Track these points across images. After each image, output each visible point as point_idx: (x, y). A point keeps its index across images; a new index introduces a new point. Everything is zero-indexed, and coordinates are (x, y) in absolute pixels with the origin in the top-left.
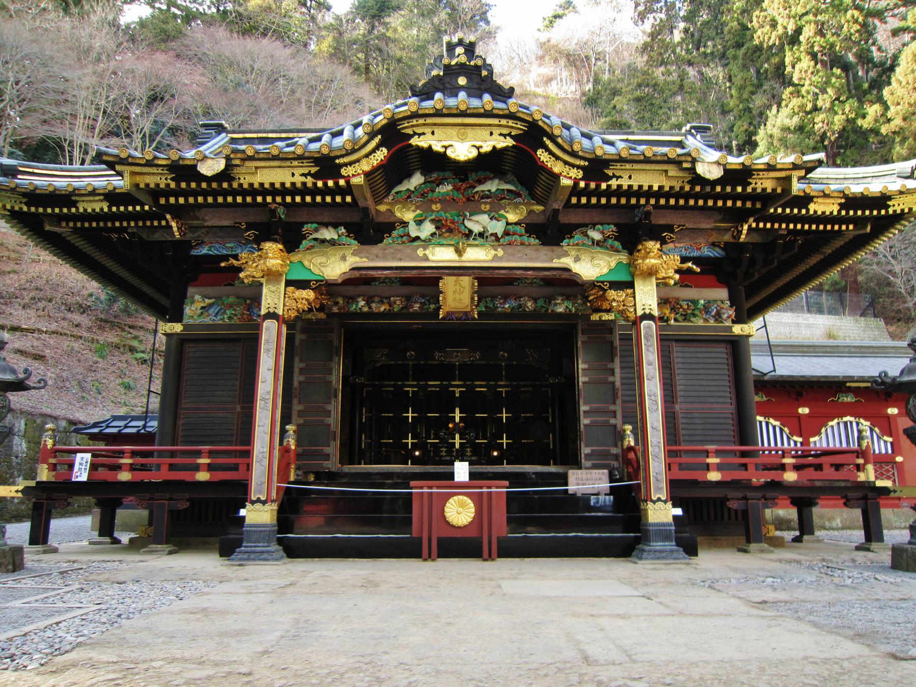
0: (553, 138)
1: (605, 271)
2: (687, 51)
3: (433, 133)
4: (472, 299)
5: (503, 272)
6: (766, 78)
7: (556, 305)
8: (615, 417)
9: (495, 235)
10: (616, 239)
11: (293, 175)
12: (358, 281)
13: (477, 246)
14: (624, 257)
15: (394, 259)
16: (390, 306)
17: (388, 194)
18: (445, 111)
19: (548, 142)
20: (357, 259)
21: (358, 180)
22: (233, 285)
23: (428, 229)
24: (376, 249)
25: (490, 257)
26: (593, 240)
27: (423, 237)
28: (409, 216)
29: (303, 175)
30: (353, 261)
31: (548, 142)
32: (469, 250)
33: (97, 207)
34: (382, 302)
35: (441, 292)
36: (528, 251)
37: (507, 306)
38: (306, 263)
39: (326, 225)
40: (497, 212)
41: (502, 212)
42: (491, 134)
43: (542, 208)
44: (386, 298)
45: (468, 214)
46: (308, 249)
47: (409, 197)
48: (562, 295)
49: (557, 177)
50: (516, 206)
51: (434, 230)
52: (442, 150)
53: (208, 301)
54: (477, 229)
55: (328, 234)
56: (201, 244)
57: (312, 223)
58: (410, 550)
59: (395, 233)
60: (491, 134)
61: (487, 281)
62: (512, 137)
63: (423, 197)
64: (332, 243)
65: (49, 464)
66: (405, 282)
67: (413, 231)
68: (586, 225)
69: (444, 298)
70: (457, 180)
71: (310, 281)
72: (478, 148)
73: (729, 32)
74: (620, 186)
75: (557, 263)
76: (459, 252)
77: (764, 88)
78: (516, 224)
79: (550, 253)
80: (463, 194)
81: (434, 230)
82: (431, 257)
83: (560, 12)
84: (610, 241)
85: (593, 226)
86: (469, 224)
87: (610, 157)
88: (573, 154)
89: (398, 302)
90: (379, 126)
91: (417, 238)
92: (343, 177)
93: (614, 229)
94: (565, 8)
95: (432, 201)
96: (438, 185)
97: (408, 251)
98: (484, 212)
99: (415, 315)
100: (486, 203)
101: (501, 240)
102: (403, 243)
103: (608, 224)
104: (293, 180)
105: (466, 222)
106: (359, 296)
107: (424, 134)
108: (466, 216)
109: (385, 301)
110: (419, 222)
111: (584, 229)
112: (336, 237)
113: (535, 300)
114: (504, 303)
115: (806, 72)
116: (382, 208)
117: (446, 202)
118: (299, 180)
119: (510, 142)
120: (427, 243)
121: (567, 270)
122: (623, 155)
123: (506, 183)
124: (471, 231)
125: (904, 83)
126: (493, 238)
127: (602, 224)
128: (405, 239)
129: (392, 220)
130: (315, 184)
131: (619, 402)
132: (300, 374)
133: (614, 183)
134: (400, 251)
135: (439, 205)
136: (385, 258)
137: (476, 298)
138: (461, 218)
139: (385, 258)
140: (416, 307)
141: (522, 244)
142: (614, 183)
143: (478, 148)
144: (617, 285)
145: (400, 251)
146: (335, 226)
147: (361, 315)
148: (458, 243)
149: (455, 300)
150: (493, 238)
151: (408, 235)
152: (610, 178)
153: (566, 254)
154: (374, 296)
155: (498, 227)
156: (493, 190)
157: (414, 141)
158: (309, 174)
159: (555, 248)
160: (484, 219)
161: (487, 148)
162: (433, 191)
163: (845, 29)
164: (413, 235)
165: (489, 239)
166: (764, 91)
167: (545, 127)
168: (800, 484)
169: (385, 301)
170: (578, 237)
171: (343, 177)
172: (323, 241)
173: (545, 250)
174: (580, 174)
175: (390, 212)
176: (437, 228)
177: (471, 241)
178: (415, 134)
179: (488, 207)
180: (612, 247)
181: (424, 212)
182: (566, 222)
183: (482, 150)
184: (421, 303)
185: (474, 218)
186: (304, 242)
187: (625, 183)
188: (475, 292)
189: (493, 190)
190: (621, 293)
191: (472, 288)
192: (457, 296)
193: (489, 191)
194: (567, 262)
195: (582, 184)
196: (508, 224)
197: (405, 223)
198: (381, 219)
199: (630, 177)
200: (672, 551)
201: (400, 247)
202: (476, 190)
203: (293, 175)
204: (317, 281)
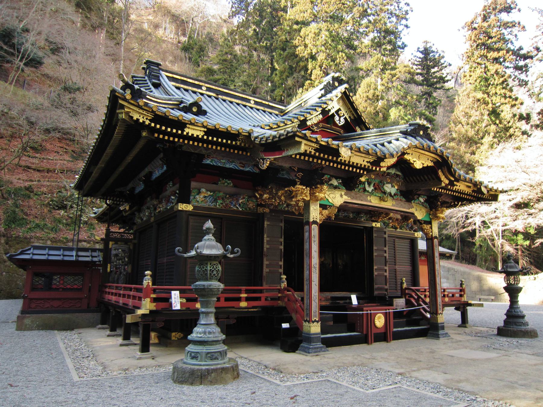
6: (295, 70)
8: (386, 272)
22: (217, 184)
33: (196, 133)
53: (209, 193)
56: (209, 156)
58: (364, 340)
65: (151, 298)
72: (423, 164)
73: (280, 41)
77: (294, 76)
115: (319, 76)
125: (362, 96)
131: (387, 265)
132: (267, 244)
143: (423, 164)
163: (338, 61)
166: (294, 78)
200: (321, 347)
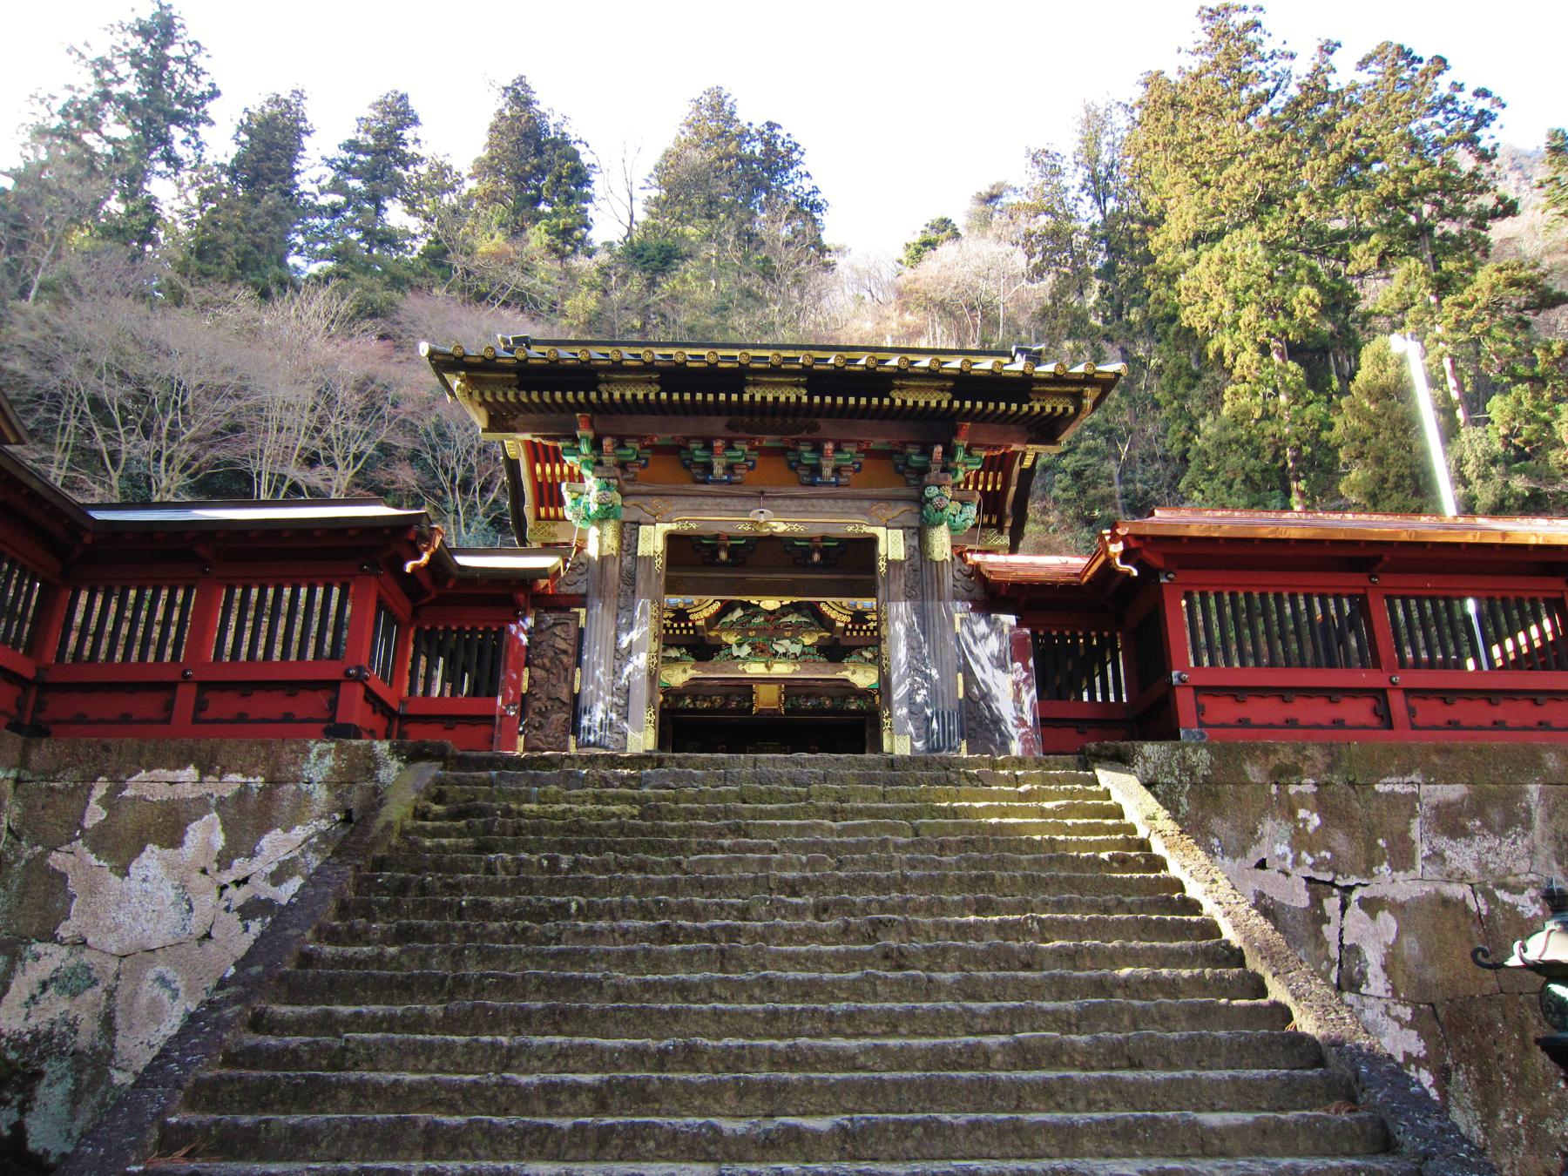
2: (1105, 321)
12: (693, 687)
23: (746, 649)
24: (708, 665)
28: (731, 639)
30: (692, 673)
49: (834, 621)
50: (810, 632)
54: (781, 650)
61: (790, 687)
63: (742, 627)
64: (676, 660)
75: (839, 675)
83: (933, 236)
85: (866, 648)
94: (939, 231)
99: (732, 711)
110: (740, 645)
113: (833, 699)
116: (713, 634)
120: (745, 660)
139: (715, 672)
140: (734, 705)
146: (678, 647)
147: (687, 711)
155: (797, 649)
160: (787, 642)
168: (506, 637)
173: (831, 666)
175: (719, 637)
192: (767, 698)
194: (846, 674)
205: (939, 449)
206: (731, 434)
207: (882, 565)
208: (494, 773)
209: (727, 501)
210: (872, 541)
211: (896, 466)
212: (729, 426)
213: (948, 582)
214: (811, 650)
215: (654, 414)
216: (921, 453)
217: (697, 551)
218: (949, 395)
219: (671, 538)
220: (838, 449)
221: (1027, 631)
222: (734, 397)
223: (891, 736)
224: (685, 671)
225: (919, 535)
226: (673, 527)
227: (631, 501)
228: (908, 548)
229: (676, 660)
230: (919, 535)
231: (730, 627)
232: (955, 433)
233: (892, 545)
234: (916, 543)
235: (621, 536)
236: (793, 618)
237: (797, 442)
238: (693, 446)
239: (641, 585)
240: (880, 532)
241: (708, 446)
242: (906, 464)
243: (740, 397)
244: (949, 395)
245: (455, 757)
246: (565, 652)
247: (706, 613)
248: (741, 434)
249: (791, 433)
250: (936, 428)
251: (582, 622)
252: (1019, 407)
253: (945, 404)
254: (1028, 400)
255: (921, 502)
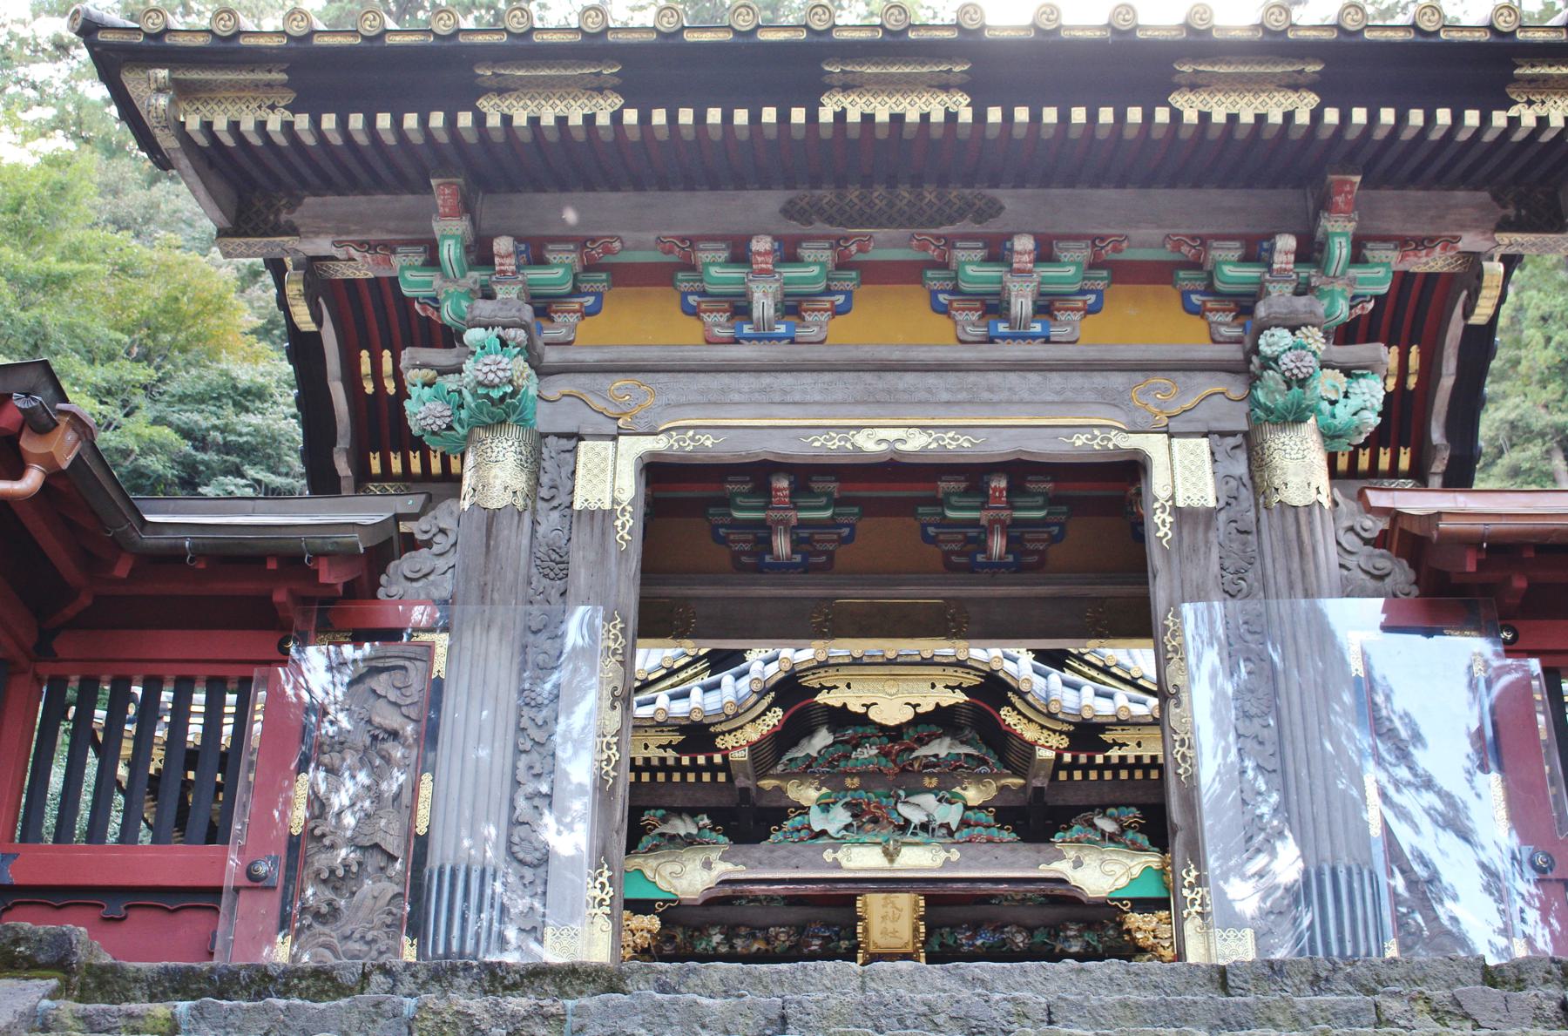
0: (1021, 695)
1: (1123, 882)
3: (849, 686)
4: (916, 929)
5: (960, 885)
7: (1067, 939)
9: (947, 826)
10: (1142, 830)
11: (646, 747)
13: (917, 844)
14: (1153, 860)
15: (787, 866)
16: (768, 943)
17: (776, 764)
18: (866, 660)
19: (1014, 699)
20: (729, 866)
21: (740, 756)
23: (840, 816)
24: (759, 851)
25: (939, 862)
26: (1103, 833)
27: (832, 831)
29: (660, 747)
30: (724, 869)
31: (1014, 699)
32: (904, 850)
34: (754, 937)
35: (861, 919)
36: (999, 851)
37: (979, 942)
38: (649, 874)
39: (678, 812)
40: (948, 790)
41: (957, 789)
42: (933, 686)
43: (1022, 781)
44: (761, 929)
45: (902, 793)
46: (650, 850)
47: (809, 766)
48: (1077, 921)
49: (1032, 745)
50: (979, 779)
51: (850, 820)
52: (863, 710)
54: (917, 817)
55: (683, 827)
57: (657, 808)
59: (788, 825)
60: (933, 686)
62: (964, 690)
63: (829, 771)
66: (792, 901)
67: (817, 821)
68: (1091, 808)
69: (866, 930)
70: (885, 740)
71: (655, 901)
74: (1123, 758)
75: (1045, 871)
76: (890, 856)
78: (980, 808)
79: (1033, 855)
80: (894, 761)
81: (850, 820)
82: (844, 863)
84: (1130, 834)
85: (1103, 809)
86: (905, 810)
87: (1104, 720)
88: (1051, 716)
89: (783, 937)
90: (773, 682)
91: (824, 833)
92: (718, 750)
93: (1137, 813)
95: (846, 774)
96: (855, 748)
97: (809, 854)
98: (929, 791)
100: (931, 775)
101: (957, 835)
102: (801, 840)
103: (1128, 806)
104: (647, 754)
105: (900, 807)
106: (713, 925)
107: (835, 687)
108: (899, 797)
109: (759, 934)
110: (826, 807)
111: (1088, 814)
112: (695, 831)
113: (1031, 931)
114: (973, 937)
116: (767, 784)
117: (869, 777)
118: (654, 754)
119: (960, 697)
120: (837, 843)
121: (1063, 881)
122: (1123, 718)
123: (962, 743)
124: (908, 822)
126: (944, 831)
127: (1116, 806)
128: (803, 833)
129: (783, 803)
130: (678, 760)
133: (1114, 754)
134: (796, 853)
135: (856, 780)
136: (772, 865)
137: (922, 929)
138: (892, 801)
141: (990, 841)
142: (1114, 754)
143: (915, 706)
144: (1145, 905)
145: (796, 853)
146: (693, 813)
148: (887, 841)
149: (884, 933)
150: (944, 831)
151: (809, 828)
152: (1109, 746)
153: (1060, 856)
154: (738, 925)
155: (952, 815)
156: (943, 754)
157: (822, 698)
158: (670, 745)
159: (1043, 846)
160: (929, 800)
161: (927, 706)
162: (847, 757)
164: (817, 828)
165: (937, 833)
167: (1009, 680)
169: (759, 934)
170: (1077, 830)
171: (718, 750)
172: (673, 838)
173: (1026, 851)
174: (1065, 742)
175: (779, 790)
176: (854, 816)
177: (908, 838)
178: (823, 687)
179: (934, 782)
180: (1133, 842)
181: (833, 790)
182: (1061, 803)
183: (919, 710)
184: (823, 938)
185: (913, 799)
186: (645, 839)
187: (1131, 753)
188: (921, 918)
189: (943, 754)
190: (1148, 917)
191: (915, 911)
193: (936, 756)
194: (1061, 868)
195: (1067, 757)
196: (967, 808)
197: (803, 808)
198: (764, 803)
199: (1139, 745)
201: (797, 847)
202: (915, 754)
203: (646, 747)
204: (665, 901)
205: (1286, 243)
206: (794, 228)
207: (1161, 524)
208: (183, 1006)
209: (786, 380)
210: (1134, 469)
211: (1185, 296)
212: (789, 212)
213: (1328, 555)
214: (982, 816)
215: (615, 188)
216: (1247, 259)
217: (723, 541)
218: (1312, 99)
219: (655, 471)
220: (1045, 254)
221: (1535, 665)
222: (798, 115)
223: (1206, 928)
224: (707, 865)
225: (1248, 446)
226: (658, 444)
227: (559, 386)
228: (1222, 479)
229: (690, 841)
230: (1248, 446)
231: (806, 771)
232: (1324, 204)
233: (1183, 475)
234: (1240, 468)
235: (534, 464)
236: (941, 748)
237: (950, 242)
238: (704, 256)
239: (581, 576)
240: (1154, 446)
241: (740, 255)
242: (1210, 291)
243: (812, 117)
244: (1312, 99)
245: (92, 970)
246: (394, 735)
247: (753, 734)
248: (820, 227)
249: (932, 223)
250: (1280, 171)
251: (440, 665)
252: (1485, 120)
253: (1302, 118)
254: (1507, 104)
255: (1248, 367)
